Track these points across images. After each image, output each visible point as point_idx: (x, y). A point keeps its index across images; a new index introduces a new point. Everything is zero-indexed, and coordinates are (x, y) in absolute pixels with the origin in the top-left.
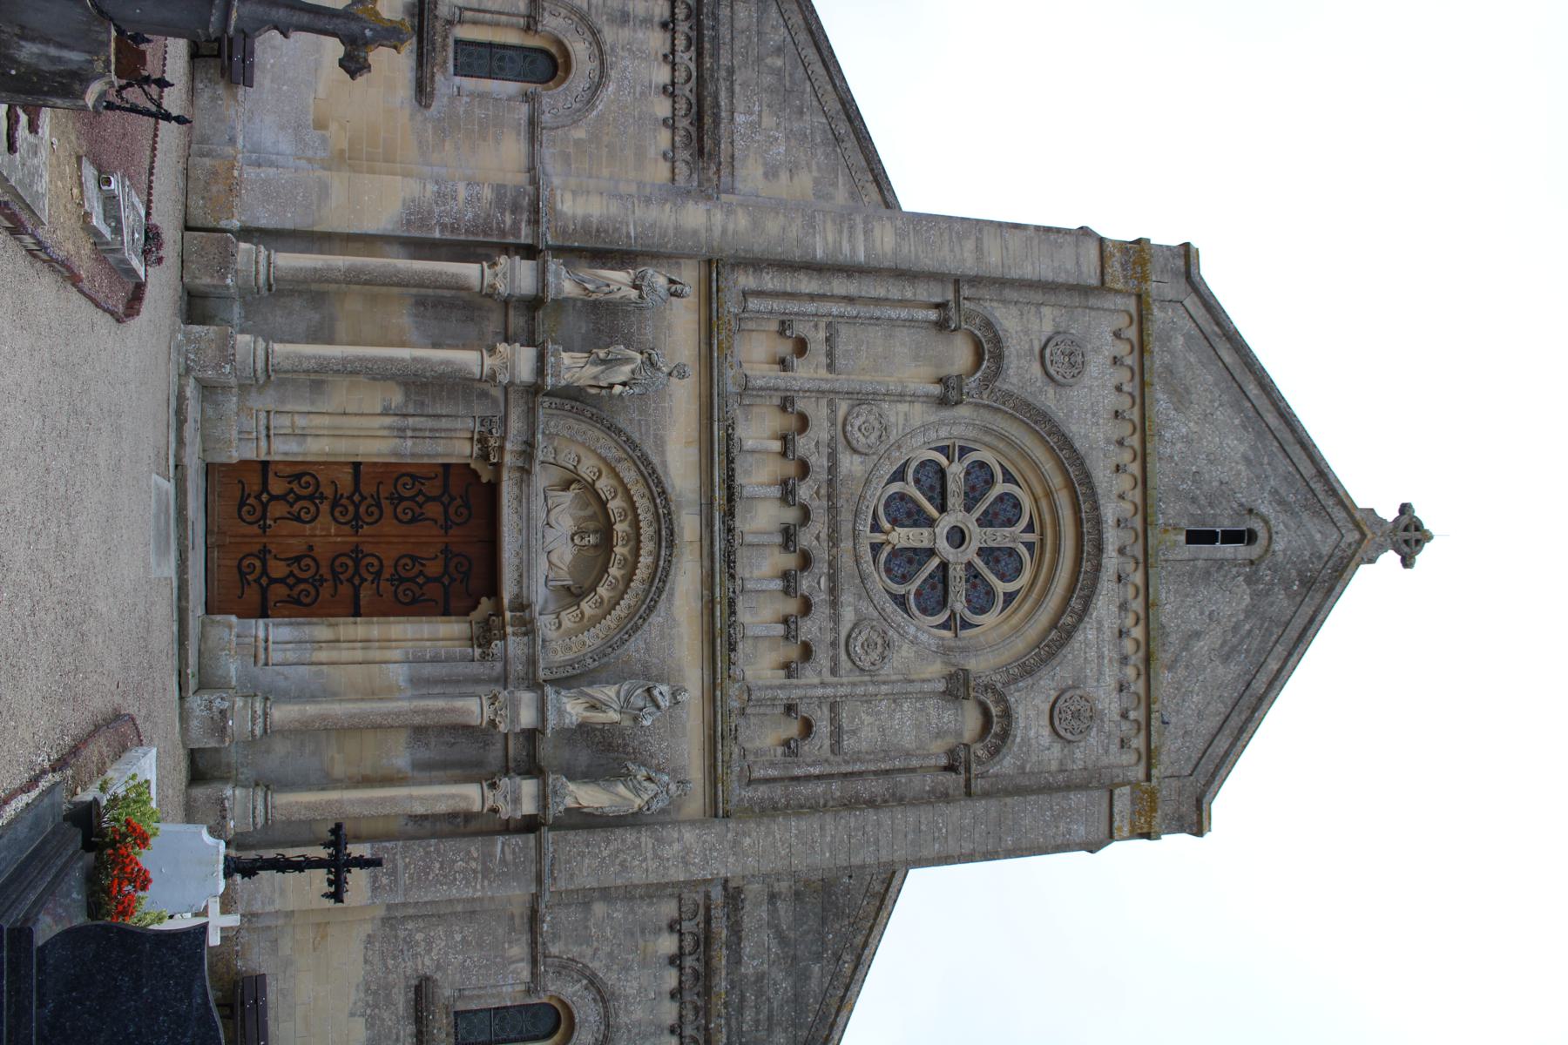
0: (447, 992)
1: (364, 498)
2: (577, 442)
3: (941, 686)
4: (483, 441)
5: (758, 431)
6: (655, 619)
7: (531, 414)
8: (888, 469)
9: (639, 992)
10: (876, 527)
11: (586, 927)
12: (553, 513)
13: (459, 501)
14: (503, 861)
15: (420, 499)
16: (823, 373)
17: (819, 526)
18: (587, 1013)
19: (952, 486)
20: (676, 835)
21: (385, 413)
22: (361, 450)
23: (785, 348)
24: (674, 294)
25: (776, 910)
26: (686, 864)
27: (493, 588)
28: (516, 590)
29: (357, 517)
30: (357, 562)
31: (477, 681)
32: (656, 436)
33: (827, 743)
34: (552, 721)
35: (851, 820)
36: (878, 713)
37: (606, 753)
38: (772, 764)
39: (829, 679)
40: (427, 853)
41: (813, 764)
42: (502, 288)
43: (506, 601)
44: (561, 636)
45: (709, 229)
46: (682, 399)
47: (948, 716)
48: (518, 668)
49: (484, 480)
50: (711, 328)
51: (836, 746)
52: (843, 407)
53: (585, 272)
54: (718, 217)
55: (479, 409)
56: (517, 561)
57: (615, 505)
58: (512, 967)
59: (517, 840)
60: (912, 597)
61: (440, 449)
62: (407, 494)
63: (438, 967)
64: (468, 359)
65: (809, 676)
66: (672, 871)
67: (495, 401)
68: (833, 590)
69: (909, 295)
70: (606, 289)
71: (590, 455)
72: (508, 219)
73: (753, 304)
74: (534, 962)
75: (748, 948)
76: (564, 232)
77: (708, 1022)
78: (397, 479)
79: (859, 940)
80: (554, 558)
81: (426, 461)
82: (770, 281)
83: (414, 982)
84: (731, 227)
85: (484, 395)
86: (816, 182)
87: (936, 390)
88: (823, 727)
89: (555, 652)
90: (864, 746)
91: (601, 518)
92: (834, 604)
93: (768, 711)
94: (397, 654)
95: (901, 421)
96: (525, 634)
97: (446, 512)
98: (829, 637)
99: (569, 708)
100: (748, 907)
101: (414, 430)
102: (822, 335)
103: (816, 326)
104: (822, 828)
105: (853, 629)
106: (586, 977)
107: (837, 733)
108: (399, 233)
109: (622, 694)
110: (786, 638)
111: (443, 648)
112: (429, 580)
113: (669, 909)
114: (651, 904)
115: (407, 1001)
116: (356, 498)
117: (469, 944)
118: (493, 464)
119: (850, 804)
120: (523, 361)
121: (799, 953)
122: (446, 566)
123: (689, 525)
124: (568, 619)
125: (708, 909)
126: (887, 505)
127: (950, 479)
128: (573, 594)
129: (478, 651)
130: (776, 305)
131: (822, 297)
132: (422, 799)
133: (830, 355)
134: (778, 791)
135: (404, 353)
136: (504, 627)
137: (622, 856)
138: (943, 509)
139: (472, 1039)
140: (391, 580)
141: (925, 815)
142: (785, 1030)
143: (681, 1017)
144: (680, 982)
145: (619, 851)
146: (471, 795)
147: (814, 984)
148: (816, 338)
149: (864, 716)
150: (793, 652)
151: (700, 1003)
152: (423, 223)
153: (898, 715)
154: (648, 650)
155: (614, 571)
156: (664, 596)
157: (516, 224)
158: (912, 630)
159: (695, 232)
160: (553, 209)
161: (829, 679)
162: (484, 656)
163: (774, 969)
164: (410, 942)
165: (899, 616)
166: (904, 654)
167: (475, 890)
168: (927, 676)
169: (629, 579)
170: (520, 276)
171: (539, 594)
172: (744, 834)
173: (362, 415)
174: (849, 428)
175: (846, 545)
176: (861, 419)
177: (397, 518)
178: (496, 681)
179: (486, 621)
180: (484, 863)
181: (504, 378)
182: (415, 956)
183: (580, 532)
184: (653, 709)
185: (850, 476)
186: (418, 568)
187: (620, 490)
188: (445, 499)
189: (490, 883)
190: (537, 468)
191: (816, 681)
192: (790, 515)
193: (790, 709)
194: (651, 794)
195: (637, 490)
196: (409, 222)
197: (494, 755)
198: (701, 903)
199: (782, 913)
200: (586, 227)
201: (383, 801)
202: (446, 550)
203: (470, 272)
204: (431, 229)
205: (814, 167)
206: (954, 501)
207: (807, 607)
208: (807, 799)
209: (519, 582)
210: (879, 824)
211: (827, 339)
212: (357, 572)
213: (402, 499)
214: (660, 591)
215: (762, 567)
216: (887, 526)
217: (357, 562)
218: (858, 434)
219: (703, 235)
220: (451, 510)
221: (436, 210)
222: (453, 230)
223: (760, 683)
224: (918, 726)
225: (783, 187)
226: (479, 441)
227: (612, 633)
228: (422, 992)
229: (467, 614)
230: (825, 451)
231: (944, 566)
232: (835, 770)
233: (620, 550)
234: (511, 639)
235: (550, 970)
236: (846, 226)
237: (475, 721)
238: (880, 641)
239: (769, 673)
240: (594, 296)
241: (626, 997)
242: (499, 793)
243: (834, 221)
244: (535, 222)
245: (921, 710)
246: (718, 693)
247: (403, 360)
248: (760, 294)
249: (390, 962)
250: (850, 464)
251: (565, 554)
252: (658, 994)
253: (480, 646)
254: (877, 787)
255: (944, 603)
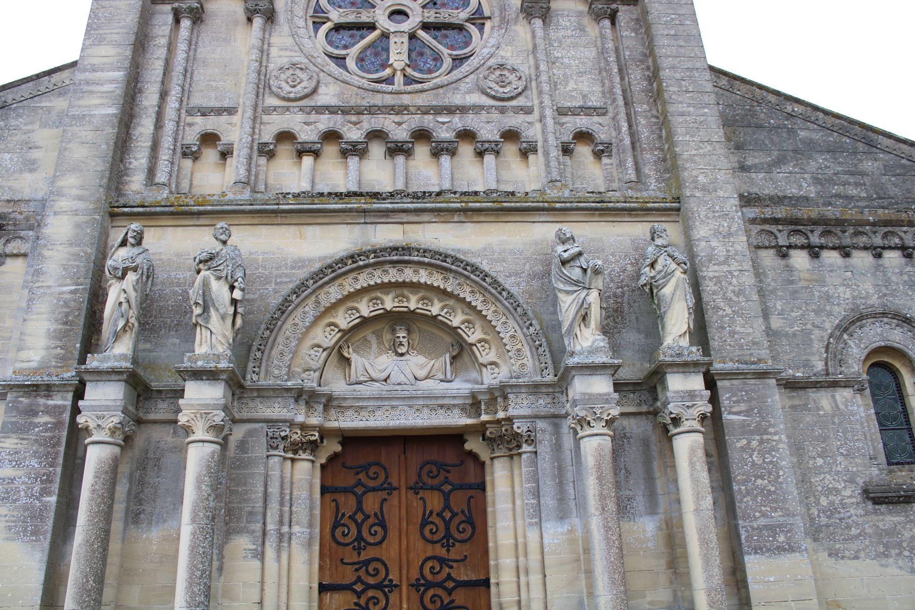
0: (875, 471)
1: (359, 580)
2: (298, 345)
3: (538, 23)
4: (295, 448)
5: (290, 176)
6: (485, 266)
7: (264, 393)
8: (333, 67)
9: (847, 286)
10: (389, 80)
11: (794, 335)
12: (374, 375)
13: (362, 476)
14: (747, 412)
15: (359, 517)
16: (236, 119)
17: (387, 122)
18: (875, 334)
19: (351, 18)
20: (703, 244)
21: (261, 556)
22: (304, 583)
23: (210, 155)
24: (139, 243)
25: (755, 166)
26: (730, 235)
27: (452, 438)
28: (457, 411)
29: (379, 587)
30: (429, 585)
31: (558, 447)
32: (293, 268)
33: (596, 119)
34: (602, 358)
35: (671, 90)
36: (565, 75)
37: (632, 307)
38: (621, 164)
39: (536, 114)
40: (748, 493)
41: (618, 129)
42: (116, 419)
43: (470, 421)
44: (506, 360)
45: (76, 213)
46: (254, 242)
47: (564, 22)
48: (542, 404)
49: (339, 448)
50: (184, 212)
51: (600, 111)
52: (272, 101)
53: (107, 329)
54: (64, 204)
55: (259, 449)
56: (426, 411)
57: (365, 308)
58: (842, 407)
59: (725, 399)
60: (454, 53)
61: (304, 494)
62: (354, 531)
63: (852, 481)
64: (197, 457)
65: (533, 132)
66: (739, 248)
67: (250, 433)
68: (450, 110)
69: (164, 41)
70: (125, 305)
71: (312, 334)
72: (43, 419)
73: (161, 177)
74: (835, 384)
75: (792, 191)
76: (63, 358)
77: (868, 223)
78: (339, 543)
79: (772, 98)
80: (422, 373)
81: (317, 512)
82: (139, 160)
83: (870, 506)
84: (75, 192)
85: (243, 445)
86: (44, 125)
87: (258, 21)
88: (582, 122)
89: (523, 365)
90: (597, 88)
91: (378, 326)
92: (463, 110)
93: (569, 170)
94: (533, 536)
95: (288, 53)
96: (505, 398)
97: (374, 490)
98: (495, 115)
99: (588, 343)
100: (754, 190)
101: (281, 523)
102: (199, 119)
103: (190, 125)
104: (682, 114)
105: (488, 95)
106: (841, 335)
107: (587, 110)
108: (46, 544)
109: (568, 288)
110: (497, 153)
111: (522, 485)
112: (447, 506)
113: (768, 258)
114: (766, 276)
115: (890, 513)
116: (359, 587)
117: (824, 450)
118: (322, 438)
119: (657, 95)
120: (202, 396)
121: (790, 148)
122: (432, 488)
123: (386, 235)
124: (486, 355)
125: (765, 221)
126: (369, 72)
127: (343, 20)
128: (461, 352)
129: (525, 448)
130: (164, 155)
131: (425, 111)
132: (698, 498)
133: (219, 111)
134: (649, 157)
135: (186, 531)
136: (498, 422)
137: (730, 295)
138: (372, 27)
139: (910, 448)
140: (448, 547)
141: (659, 31)
142: (861, 161)
143: (865, 248)
144: (834, 248)
145: (725, 298)
146: (688, 446)
147: (817, 136)
148: (202, 124)
149: (569, 88)
150: (510, 150)
151: (851, 230)
152: (37, 515)
153: (566, 61)
154: (517, 274)
155: (435, 309)
156: (462, 257)
157: (48, 411)
158: (486, 51)
159: (77, 226)
160: (35, 371)
161: (536, 114)
162: (531, 441)
163: (808, 169)
164: (831, 511)
165: (473, 62)
166: (509, 54)
167: (780, 441)
168: (529, 36)
169: (443, 293)
170: (105, 400)
171: (461, 387)
172: (695, 181)
173: (262, 582)
174: (292, 96)
175: (406, 99)
176: (284, 85)
177: (380, 543)
178: (557, 428)
179: (491, 442)
180: (752, 433)
181: (219, 417)
182: (844, 506)
183: (394, 347)
184: (582, 259)
185: (340, 95)
186: (435, 519)
187: (350, 304)
188: (359, 490)
189: (770, 425)
190: (324, 389)
191: (538, 126)
192: (377, 150)
193: (566, 150)
194: (670, 260)
195: (349, 285)
196: (35, 533)
197: (636, 427)
198: (759, 227)
199: (757, 161)
200: (61, 336)
201: (704, 542)
202: (415, 489)
203: (95, 457)
204: (45, 506)
205: (30, 127)
206: (365, 18)
207: (467, 135)
208: (652, 132)
209: (449, 408)
210: (673, 67)
211: (203, 115)
212: (440, 585)
213: (360, 538)
214: (456, 260)
215: (425, 173)
216: (388, 71)
217: (429, 585)
218: (299, 88)
219: (81, 219)
220: (372, 484)
221: (23, 500)
222: (50, 481)
223: (543, 175)
224: (575, 46)
225: (45, 156)
226: (295, 452)
227: (501, 309)
228: (879, 498)
229: (483, 464)
230: (313, 117)
231: (426, 26)
232: (622, 110)
233: (413, 303)
234: (512, 412)
235: (839, 369)
236: (86, 88)
237: (607, 442)
238: (498, 73)
239: (533, 169)
240: (133, 320)
241: (854, 298)
242: (686, 414)
243: (79, 99)
244: (48, 389)
245: (560, 42)
246: (558, 205)
247: (193, 534)
248: (151, 172)
249: (854, 531)
250: (328, 95)
251: (417, 363)
252: (846, 268)
253: (519, 447)
254: (636, 76)
255: (460, 28)
